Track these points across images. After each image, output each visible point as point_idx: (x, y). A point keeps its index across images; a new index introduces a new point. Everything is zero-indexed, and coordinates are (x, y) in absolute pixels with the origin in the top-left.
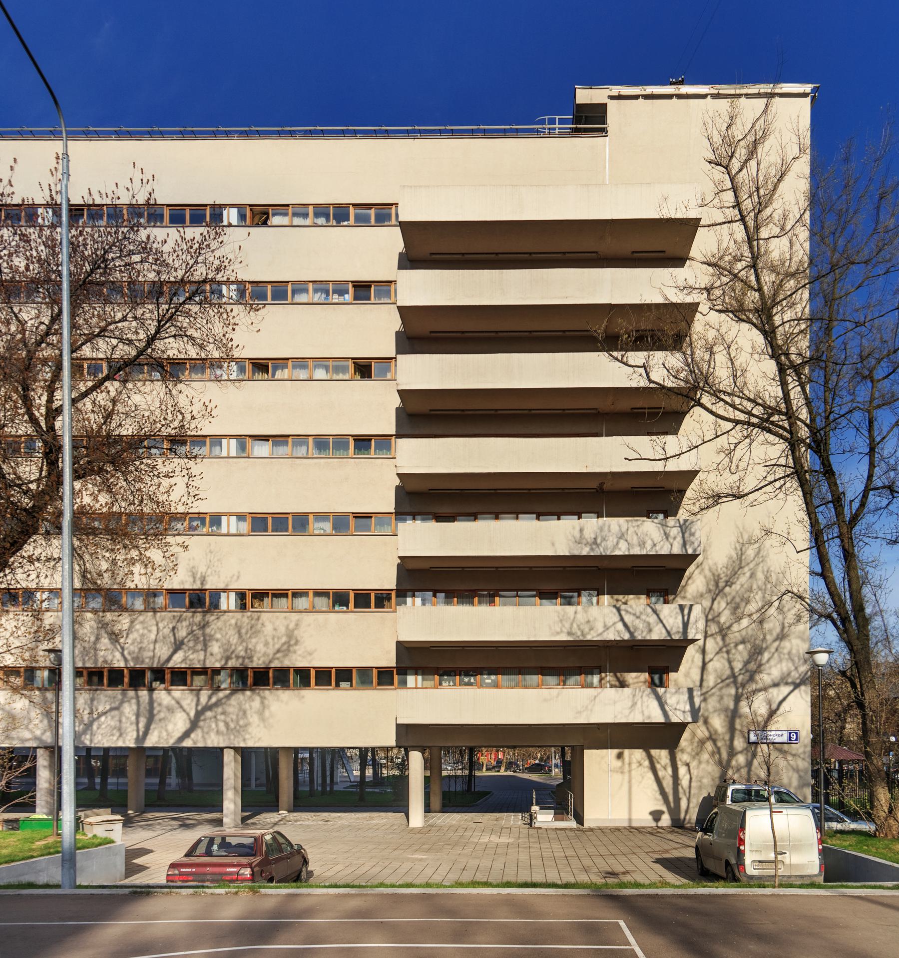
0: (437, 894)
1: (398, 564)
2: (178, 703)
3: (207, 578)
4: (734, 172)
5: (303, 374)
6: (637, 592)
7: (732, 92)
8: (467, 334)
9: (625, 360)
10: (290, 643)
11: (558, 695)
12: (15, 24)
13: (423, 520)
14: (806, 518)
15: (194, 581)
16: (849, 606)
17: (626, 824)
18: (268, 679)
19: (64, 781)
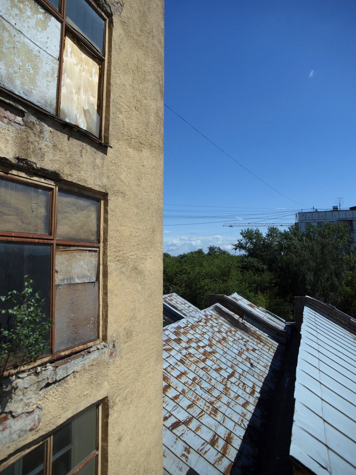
0: (65, 27)
1: (200, 252)
2: (174, 367)
3: (100, 154)
4: (205, 345)
5: (286, 224)
6: (245, 433)
7: (271, 321)
8: (21, 178)
9: (245, 390)
10: (34, 365)
11: (114, 41)
12: (312, 393)
13: (34, 188)
14: (70, 179)
15: (178, 407)
16: (248, 325)
17: (354, 229)
18: (44, 461)
19: (100, 307)
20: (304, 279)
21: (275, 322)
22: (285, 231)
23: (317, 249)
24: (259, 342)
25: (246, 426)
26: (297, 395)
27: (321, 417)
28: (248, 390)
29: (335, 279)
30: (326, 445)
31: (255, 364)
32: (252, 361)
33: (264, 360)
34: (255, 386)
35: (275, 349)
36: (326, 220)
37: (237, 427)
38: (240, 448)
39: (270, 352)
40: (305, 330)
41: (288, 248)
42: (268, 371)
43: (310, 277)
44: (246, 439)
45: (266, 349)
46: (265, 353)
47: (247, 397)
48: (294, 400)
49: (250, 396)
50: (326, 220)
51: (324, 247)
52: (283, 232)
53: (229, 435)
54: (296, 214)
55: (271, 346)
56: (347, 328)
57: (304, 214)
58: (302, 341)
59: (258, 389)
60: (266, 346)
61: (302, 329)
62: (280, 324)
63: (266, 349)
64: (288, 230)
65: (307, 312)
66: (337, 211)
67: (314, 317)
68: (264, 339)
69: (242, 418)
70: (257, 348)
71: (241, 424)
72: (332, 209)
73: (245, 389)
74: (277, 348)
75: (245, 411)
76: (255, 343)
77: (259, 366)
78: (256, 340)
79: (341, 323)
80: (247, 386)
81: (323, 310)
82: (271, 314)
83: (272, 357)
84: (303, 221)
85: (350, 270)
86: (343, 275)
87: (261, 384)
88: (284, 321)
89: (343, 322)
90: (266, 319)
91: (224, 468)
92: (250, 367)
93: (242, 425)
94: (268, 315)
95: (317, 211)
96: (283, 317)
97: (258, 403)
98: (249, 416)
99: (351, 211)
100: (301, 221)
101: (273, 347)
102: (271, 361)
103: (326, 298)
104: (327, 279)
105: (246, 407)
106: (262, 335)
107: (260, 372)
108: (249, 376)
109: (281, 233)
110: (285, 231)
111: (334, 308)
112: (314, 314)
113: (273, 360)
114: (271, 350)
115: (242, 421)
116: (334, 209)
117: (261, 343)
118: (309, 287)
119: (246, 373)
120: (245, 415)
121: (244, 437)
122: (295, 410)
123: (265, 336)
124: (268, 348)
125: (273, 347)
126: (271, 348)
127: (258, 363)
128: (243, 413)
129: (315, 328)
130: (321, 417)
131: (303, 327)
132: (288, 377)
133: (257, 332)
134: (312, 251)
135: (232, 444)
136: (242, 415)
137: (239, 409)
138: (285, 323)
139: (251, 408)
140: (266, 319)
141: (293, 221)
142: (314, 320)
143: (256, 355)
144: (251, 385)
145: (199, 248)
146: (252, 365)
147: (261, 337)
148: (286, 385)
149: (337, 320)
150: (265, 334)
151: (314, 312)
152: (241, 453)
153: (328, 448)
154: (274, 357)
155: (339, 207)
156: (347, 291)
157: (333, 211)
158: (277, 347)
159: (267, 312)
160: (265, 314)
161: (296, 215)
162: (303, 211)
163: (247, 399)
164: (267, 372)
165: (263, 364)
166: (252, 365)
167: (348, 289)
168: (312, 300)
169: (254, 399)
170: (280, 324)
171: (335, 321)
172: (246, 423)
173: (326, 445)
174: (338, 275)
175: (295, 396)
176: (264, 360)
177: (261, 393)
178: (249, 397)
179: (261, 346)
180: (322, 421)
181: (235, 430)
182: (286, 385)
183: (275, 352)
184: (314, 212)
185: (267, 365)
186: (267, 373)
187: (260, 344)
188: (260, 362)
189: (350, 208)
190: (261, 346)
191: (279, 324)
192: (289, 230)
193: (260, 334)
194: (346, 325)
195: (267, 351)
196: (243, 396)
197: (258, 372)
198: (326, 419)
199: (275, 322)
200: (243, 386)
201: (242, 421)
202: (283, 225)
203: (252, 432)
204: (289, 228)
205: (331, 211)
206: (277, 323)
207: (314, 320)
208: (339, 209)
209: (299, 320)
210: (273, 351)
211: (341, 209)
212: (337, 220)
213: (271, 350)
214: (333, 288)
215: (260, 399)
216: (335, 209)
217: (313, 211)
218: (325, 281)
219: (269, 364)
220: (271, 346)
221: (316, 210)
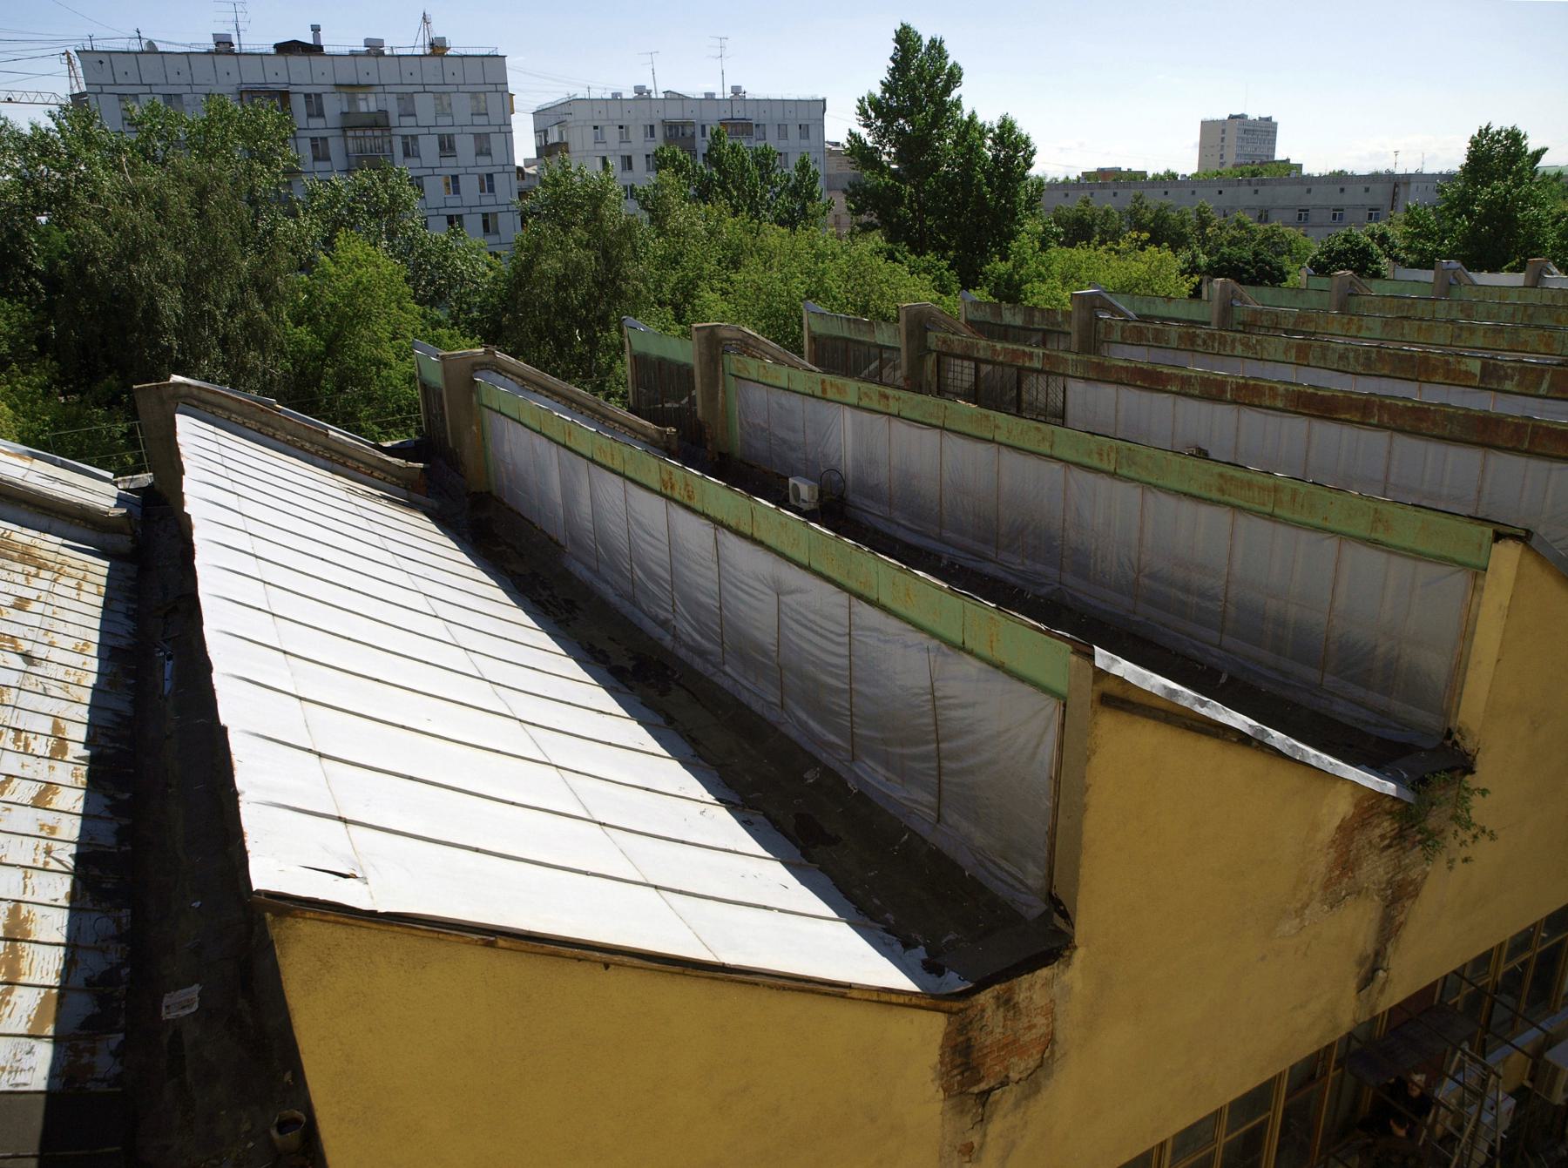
7: (57, 486)
20: (152, 313)
21: (74, 486)
22: (34, 127)
23: (179, 199)
24: (33, 570)
25: (71, 863)
26: (227, 714)
27: (310, 751)
28: (41, 746)
29: (259, 306)
30: (340, 819)
31: (39, 651)
32: (25, 646)
33: (71, 629)
34: (63, 723)
35: (103, 581)
36: (195, 89)
37: (37, 878)
38: (69, 938)
39: (84, 597)
40: (196, 498)
41: (59, 201)
42: (96, 661)
43: (171, 304)
44: (77, 904)
45: (65, 587)
46: (67, 605)
47: (42, 770)
48: (224, 731)
49: (52, 763)
50: (195, 89)
51: (202, 193)
52: (27, 131)
53: (14, 913)
54: (67, 53)
55: (81, 574)
56: (322, 461)
57: (105, 58)
58: (197, 537)
59: (79, 733)
60: (62, 580)
61: (186, 497)
62: (97, 492)
63: (65, 587)
64: (46, 123)
65: (190, 432)
66: (232, 53)
67: (215, 447)
68: (51, 556)
69: (43, 843)
70: (32, 594)
71: (46, 863)
72: (213, 47)
73: (26, 746)
74: (109, 577)
75: (47, 817)
76: (21, 579)
77: (55, 655)
78: (19, 567)
79: (302, 448)
80: (31, 736)
81: (240, 420)
82: (53, 462)
83: (98, 612)
84: (106, 89)
85: (301, 269)
86: (280, 283)
87: (83, 713)
88: (110, 475)
89: (307, 445)
90: (40, 481)
91: (25, 1019)
92: (23, 666)
93: (54, 865)
94: (39, 465)
95: (152, 50)
96: (100, 461)
97: (91, 776)
98: (71, 828)
99: (281, 59)
100: (98, 89)
101: (90, 577)
102: (97, 624)
103: (237, 376)
104: (230, 307)
105: (50, 802)
106: (38, 542)
107: (67, 673)
108: (27, 700)
109: (17, 137)
110: (34, 127)
111: (271, 405)
112: (212, 436)
113: (103, 620)
114: (85, 586)
115: (48, 852)
116: (217, 44)
117: (43, 574)
118: (170, 340)
119: (14, 692)
120: (53, 829)
121: (73, 896)
122: (235, 758)
123: (48, 544)
124: (73, 583)
125: (90, 577)
126: (84, 579)
127: (51, 645)
128: (42, 827)
129: (227, 484)
130: (310, 751)
131: (189, 486)
132: (169, 658)
133: (15, 536)
134: (161, 207)
135: (32, 938)
136: (43, 834)
137: (27, 820)
138: (115, 484)
139: (72, 799)
140: (40, 481)
141: (61, 85)
142: (218, 458)
143: (35, 620)
144: (45, 725)
145: (1477, 769)
146: (27, 657)
147: (37, 552)
148: (168, 686)
149: (287, 442)
150: (49, 537)
151: (211, 428)
152: (74, 947)
153: (346, 821)
154: (105, 607)
155: (235, 40)
156: (300, 343)
157: (217, 52)
158: (106, 571)
159: (35, 456)
160: (27, 464)
161: (70, 62)
162: (100, 46)
163: (44, 775)
164: (94, 665)
165: (70, 643)
166: (27, 657)
167: (302, 332)
168: (199, 388)
169: (72, 767)
170: (97, 492)
171: (282, 446)
172: (66, 853)
173: (340, 819)
174: (264, 289)
175: (223, 721)
176: (71, 629)
177: (87, 744)
178: (51, 768)
179: (45, 585)
180: (315, 757)
181: (29, 890)
182: (168, 686)
183: (103, 590)
184: (142, 52)
185: (87, 642)
186: (95, 668)
187: (36, 576)
188: (57, 639)
189: (276, 46)
190: (45, 585)
191: (93, 492)
192: (52, 125)
193: (27, 540)
194: (316, 453)
195: (73, 593)
196: (28, 773)
197: (60, 673)
198: (323, 751)
199: (74, 486)
200: (16, 740)
201: (48, 852)
202: (16, 97)
203: (99, 875)
204: (51, 115)
205: (209, 53)
206: (83, 489)
207: (218, 458)
208: (236, 47)
209: (170, 467)
210: (94, 589)
211: (246, 48)
212: (233, 89)
213: (85, 586)
214: (257, 336)
215: (93, 761)
216: (224, 46)
217: (137, 48)
218: (225, 316)
219: (95, 637)
220: (81, 574)
221: (150, 43)
